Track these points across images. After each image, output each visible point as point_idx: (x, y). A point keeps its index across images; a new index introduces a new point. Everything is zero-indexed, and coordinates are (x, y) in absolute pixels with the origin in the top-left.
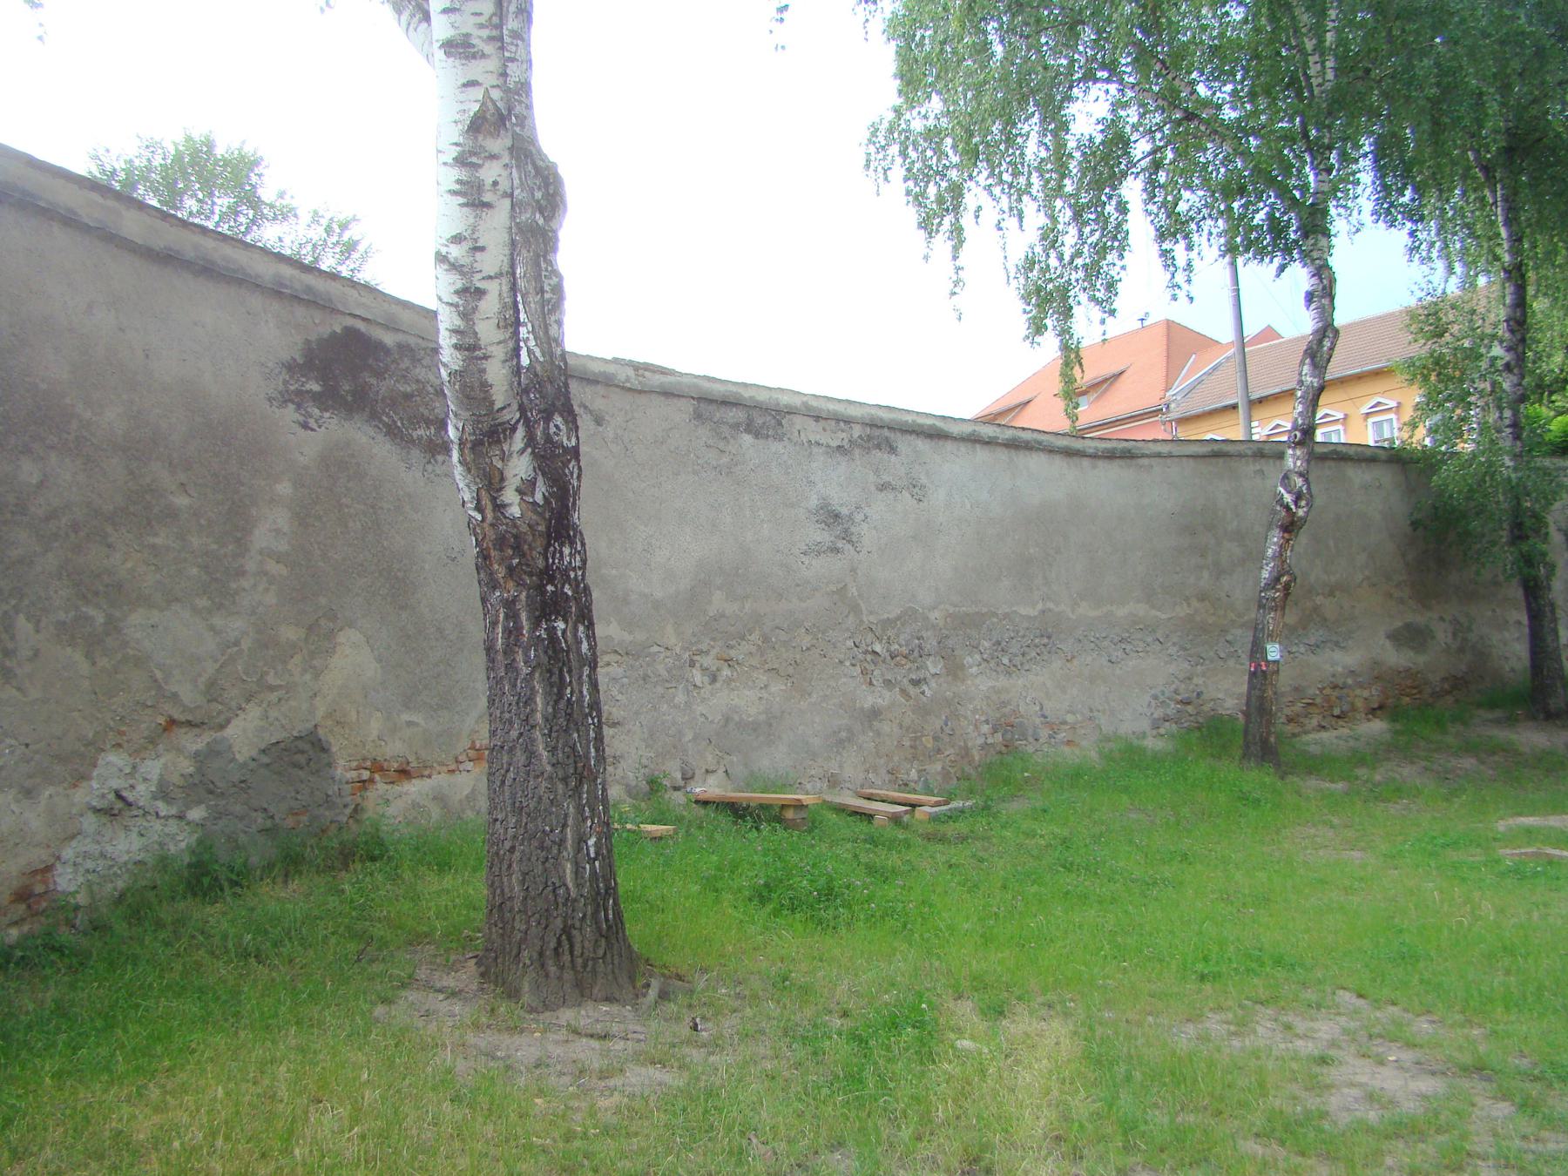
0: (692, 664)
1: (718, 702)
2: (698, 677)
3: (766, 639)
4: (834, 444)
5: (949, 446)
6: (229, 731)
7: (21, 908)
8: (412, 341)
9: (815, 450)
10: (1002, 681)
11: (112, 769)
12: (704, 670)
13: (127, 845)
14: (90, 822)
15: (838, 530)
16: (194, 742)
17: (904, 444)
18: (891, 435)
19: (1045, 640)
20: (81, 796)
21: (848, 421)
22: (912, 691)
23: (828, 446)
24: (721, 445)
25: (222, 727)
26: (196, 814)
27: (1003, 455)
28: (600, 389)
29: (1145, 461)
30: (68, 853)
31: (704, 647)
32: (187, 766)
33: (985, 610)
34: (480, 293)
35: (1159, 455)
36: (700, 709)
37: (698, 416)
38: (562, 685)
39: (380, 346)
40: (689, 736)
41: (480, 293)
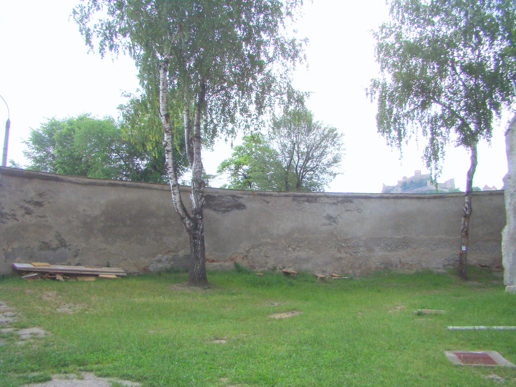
0: (289, 247)
1: (294, 255)
2: (290, 249)
3: (309, 242)
4: (332, 202)
5: (373, 200)
6: (179, 253)
7: (144, 271)
8: (222, 194)
9: (326, 204)
10: (387, 253)
11: (159, 256)
12: (292, 248)
13: (160, 265)
14: (155, 262)
15: (332, 220)
16: (173, 254)
17: (356, 201)
18: (352, 199)
19: (405, 244)
20: (154, 259)
21: (337, 197)
22: (353, 254)
23: (330, 203)
24: (299, 205)
25: (178, 252)
26: (172, 263)
27: (392, 201)
28: (269, 197)
29: (448, 198)
30: (151, 265)
31: (292, 243)
32: (171, 257)
33: (382, 237)
34: (176, 204)
35: (452, 197)
36: (290, 255)
37: (294, 200)
38: (195, 248)
39: (215, 197)
40: (286, 260)
41: (176, 204)
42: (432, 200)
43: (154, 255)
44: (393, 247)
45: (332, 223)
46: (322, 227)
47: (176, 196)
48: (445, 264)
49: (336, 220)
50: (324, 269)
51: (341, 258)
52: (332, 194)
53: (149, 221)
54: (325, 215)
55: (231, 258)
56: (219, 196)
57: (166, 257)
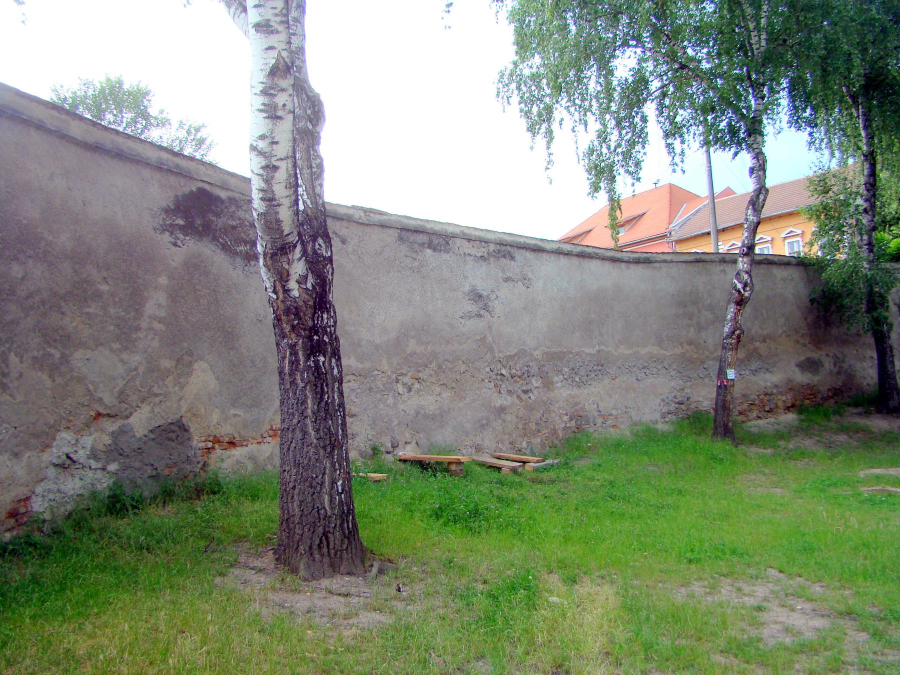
0: (397, 381)
1: (411, 403)
2: (400, 388)
3: (440, 367)
6: (131, 420)
7: (12, 521)
8: (237, 196)
10: (576, 391)
11: (64, 442)
12: (404, 384)
13: (73, 485)
14: (52, 472)
15: (481, 304)
16: (111, 426)
17: (519, 255)
18: (511, 250)
23: (475, 256)
25: (127, 417)
26: (113, 467)
27: (575, 261)
28: (345, 223)
29: (657, 265)
30: (39, 490)
31: (404, 371)
33: (565, 350)
34: (276, 168)
35: (665, 261)
37: (401, 239)
39: (218, 199)
40: (396, 423)
41: (276, 168)
42: (632, 266)
43: (45, 440)
44: (583, 376)
45: (482, 312)
46: (463, 321)
47: (280, 124)
48: (663, 411)
49: (490, 304)
50: (478, 440)
51: (502, 409)
52: (477, 233)
53: (17, 271)
54: (467, 288)
55: (271, 429)
56: (231, 199)
57: (88, 441)
